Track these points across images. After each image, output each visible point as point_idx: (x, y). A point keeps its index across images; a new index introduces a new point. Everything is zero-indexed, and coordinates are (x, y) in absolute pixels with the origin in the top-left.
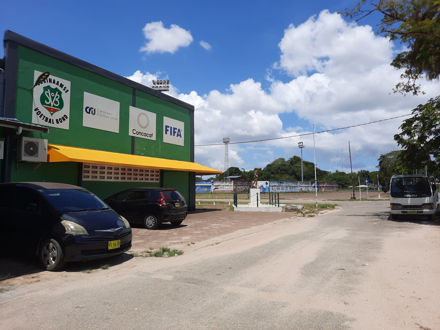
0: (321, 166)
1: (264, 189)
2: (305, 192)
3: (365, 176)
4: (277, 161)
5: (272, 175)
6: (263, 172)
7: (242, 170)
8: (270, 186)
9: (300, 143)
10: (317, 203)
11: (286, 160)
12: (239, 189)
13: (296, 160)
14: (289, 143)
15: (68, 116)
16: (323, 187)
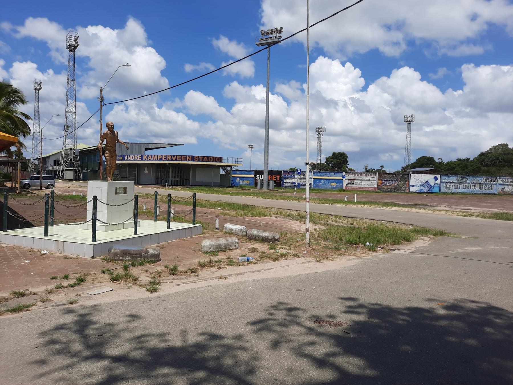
1: (431, 187)
5: (485, 168)
8: (441, 182)
10: (307, 230)
12: (386, 185)
15: (434, 176)
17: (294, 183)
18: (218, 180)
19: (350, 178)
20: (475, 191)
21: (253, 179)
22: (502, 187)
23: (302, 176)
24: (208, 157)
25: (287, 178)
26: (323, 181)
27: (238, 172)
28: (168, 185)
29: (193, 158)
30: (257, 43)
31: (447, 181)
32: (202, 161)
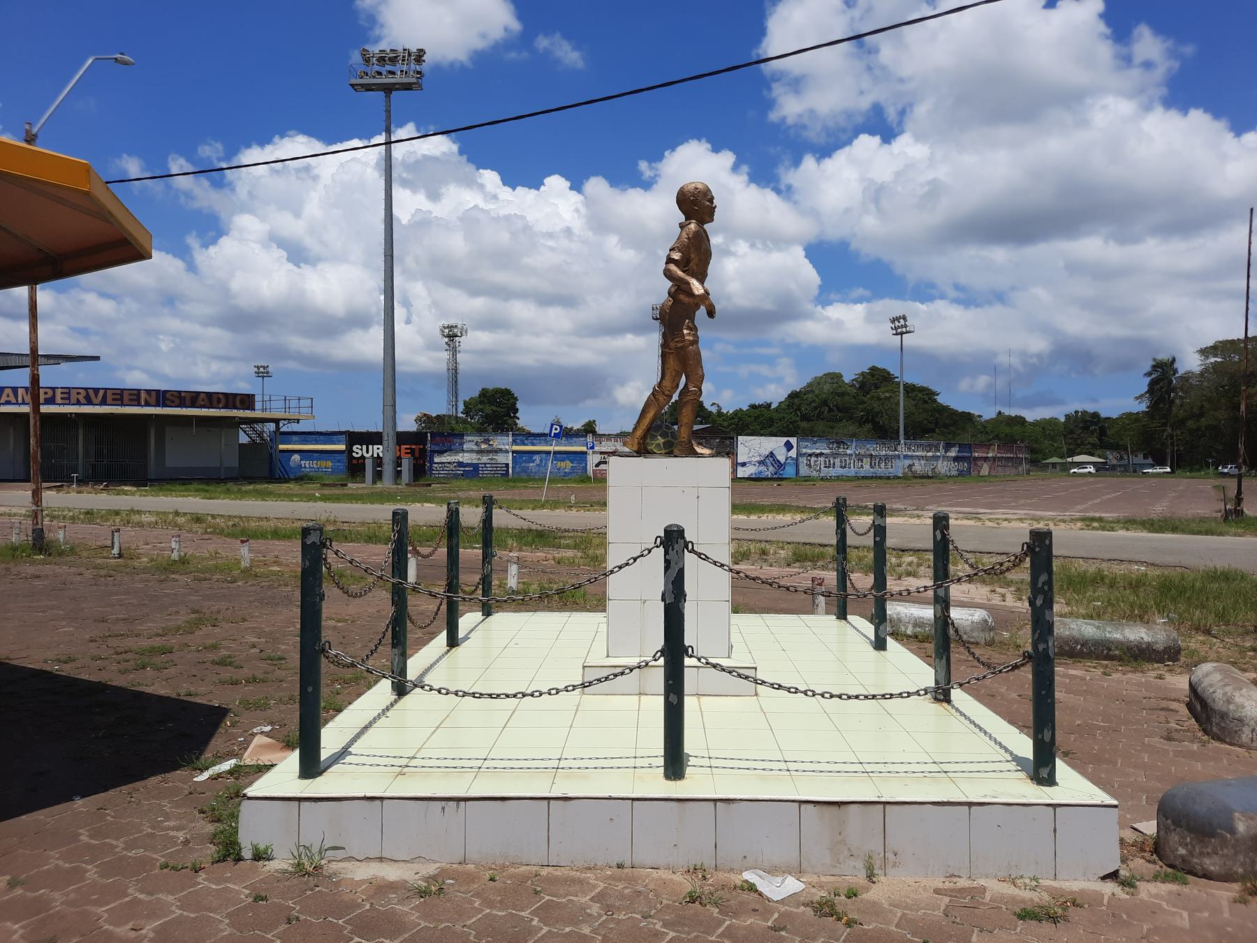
0: (957, 396)
2: (922, 477)
3: (1088, 432)
4: (818, 382)
5: (804, 424)
6: (776, 416)
7: (714, 410)
8: (799, 454)
9: (898, 319)
11: (847, 379)
13: (877, 379)
14: (850, 330)
15: (785, 439)
16: (986, 459)
17: (460, 464)
18: (233, 461)
19: (603, 449)
20: (862, 473)
21: (344, 457)
22: (910, 462)
23: (484, 446)
24: (209, 395)
25: (441, 453)
26: (537, 457)
27: (295, 438)
28: (81, 482)
29: (161, 397)
30: (354, 81)
31: (809, 451)
32: (193, 406)
